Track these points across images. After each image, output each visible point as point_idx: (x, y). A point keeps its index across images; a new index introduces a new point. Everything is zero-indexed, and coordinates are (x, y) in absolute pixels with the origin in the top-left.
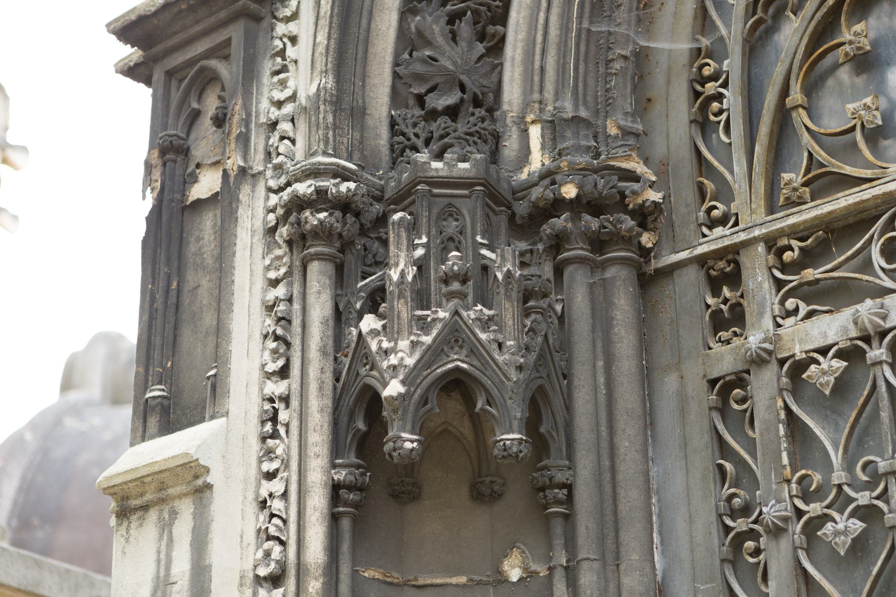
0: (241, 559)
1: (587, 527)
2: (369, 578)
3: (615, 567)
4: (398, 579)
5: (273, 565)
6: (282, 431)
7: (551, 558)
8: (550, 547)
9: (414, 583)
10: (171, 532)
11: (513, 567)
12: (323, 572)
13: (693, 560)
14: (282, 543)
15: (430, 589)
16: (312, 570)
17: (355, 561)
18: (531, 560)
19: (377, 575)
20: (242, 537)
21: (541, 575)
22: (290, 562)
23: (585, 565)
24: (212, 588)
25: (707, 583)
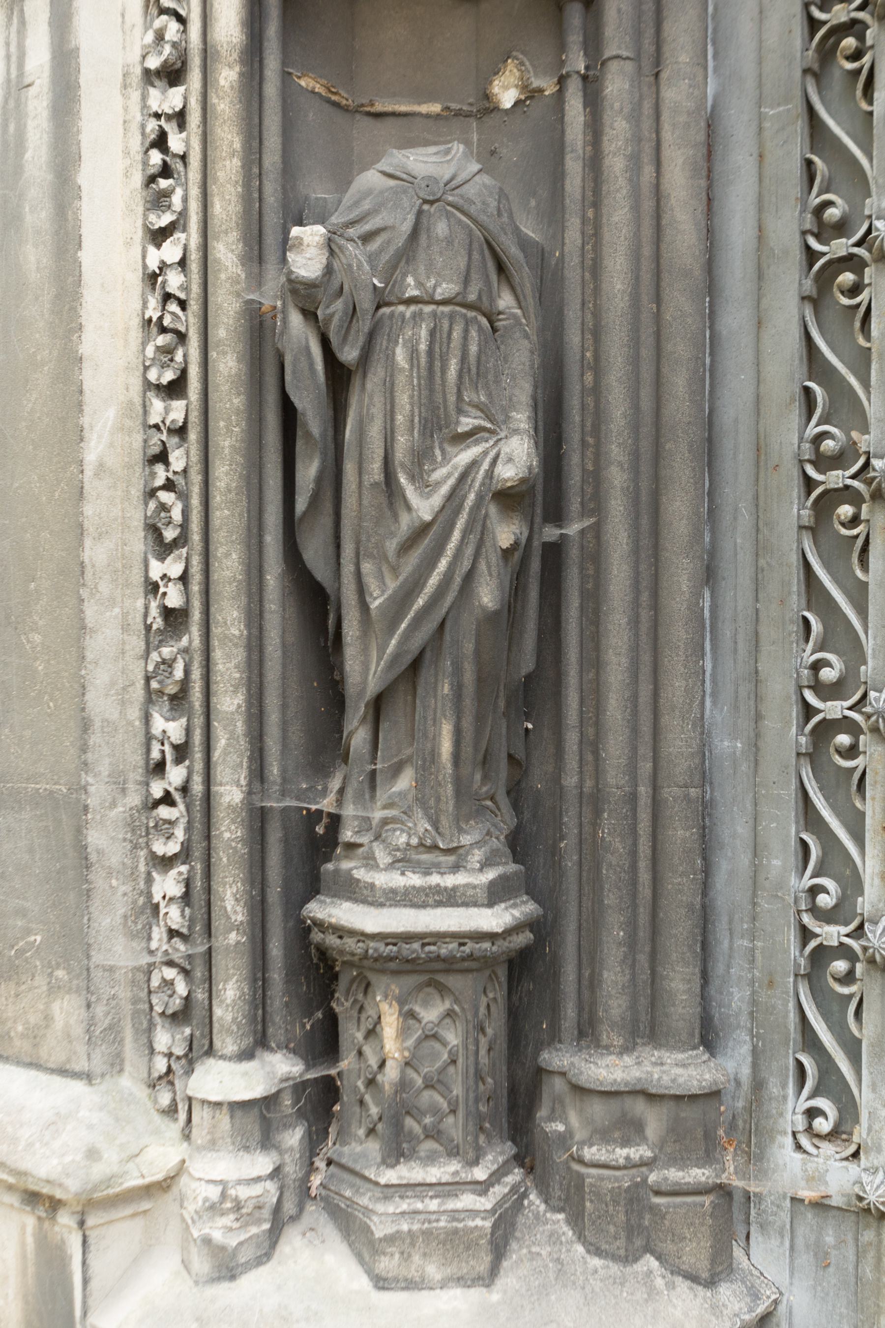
0: (124, 48)
1: (619, 11)
2: (307, 90)
3: (652, 79)
4: (347, 100)
5: (167, 49)
6: (178, 166)
7: (562, 63)
8: (562, 47)
9: (368, 109)
10: (22, 11)
11: (506, 88)
12: (240, 57)
13: (760, 75)
14: (181, 20)
15: (390, 121)
16: (223, 53)
17: (285, 61)
18: (532, 74)
19: (318, 89)
20: (123, 16)
21: (547, 93)
22: (192, 46)
23: (614, 66)
24: (82, 81)
25: (779, 105)
